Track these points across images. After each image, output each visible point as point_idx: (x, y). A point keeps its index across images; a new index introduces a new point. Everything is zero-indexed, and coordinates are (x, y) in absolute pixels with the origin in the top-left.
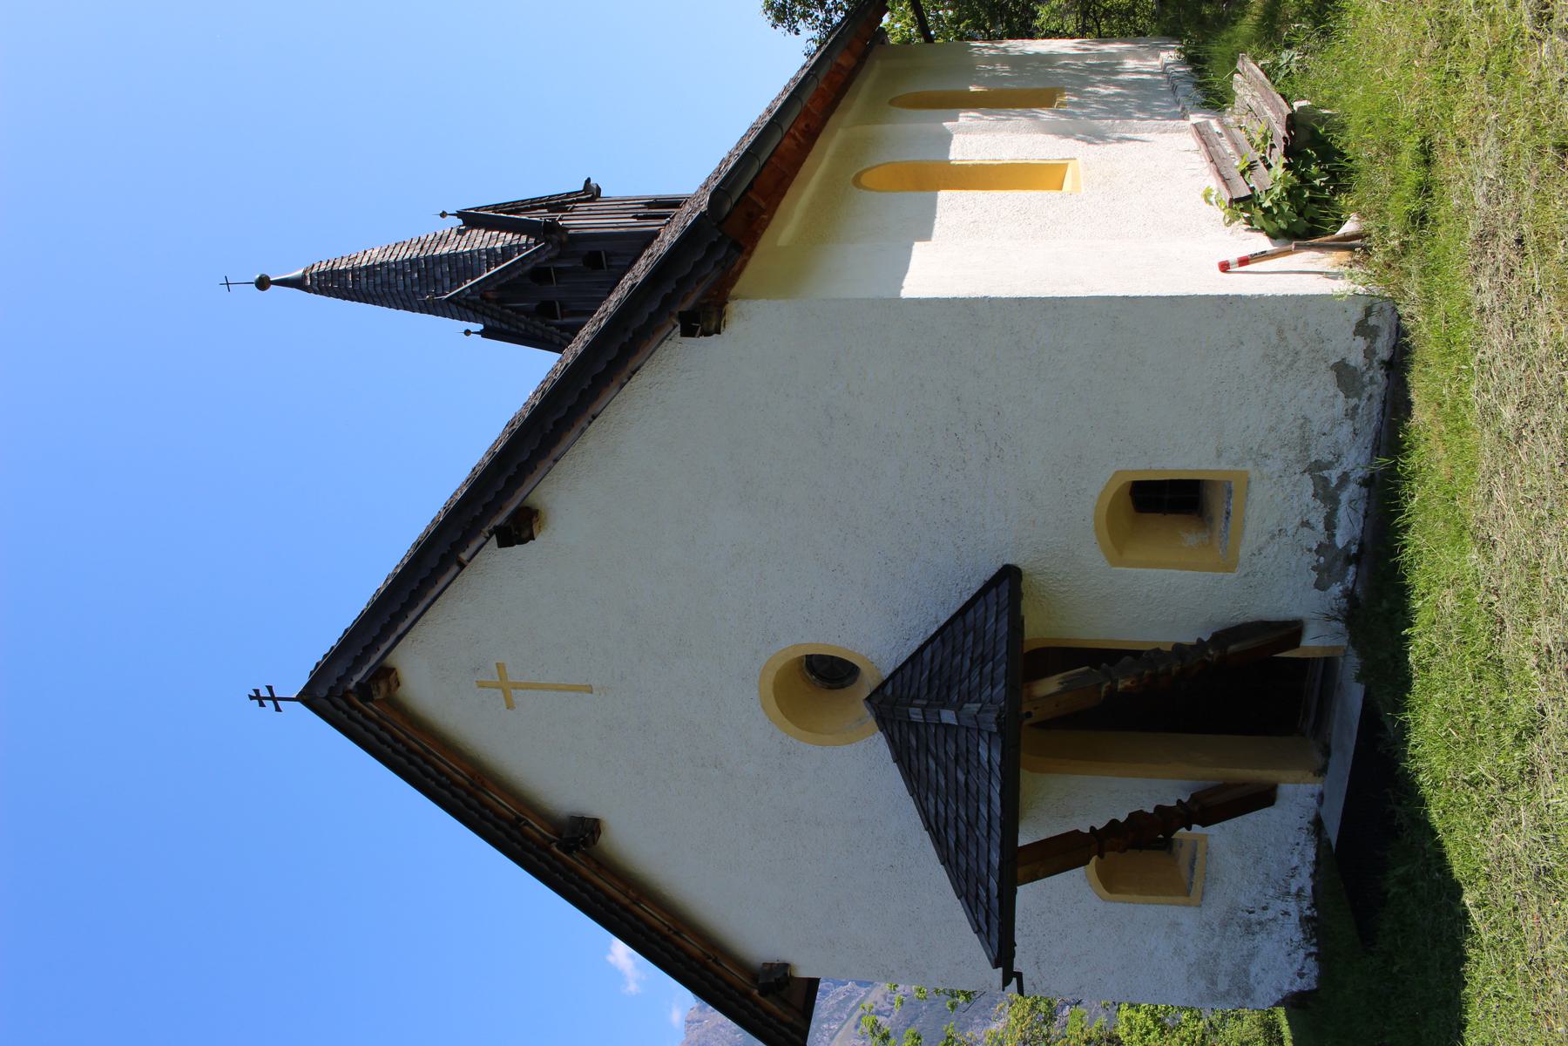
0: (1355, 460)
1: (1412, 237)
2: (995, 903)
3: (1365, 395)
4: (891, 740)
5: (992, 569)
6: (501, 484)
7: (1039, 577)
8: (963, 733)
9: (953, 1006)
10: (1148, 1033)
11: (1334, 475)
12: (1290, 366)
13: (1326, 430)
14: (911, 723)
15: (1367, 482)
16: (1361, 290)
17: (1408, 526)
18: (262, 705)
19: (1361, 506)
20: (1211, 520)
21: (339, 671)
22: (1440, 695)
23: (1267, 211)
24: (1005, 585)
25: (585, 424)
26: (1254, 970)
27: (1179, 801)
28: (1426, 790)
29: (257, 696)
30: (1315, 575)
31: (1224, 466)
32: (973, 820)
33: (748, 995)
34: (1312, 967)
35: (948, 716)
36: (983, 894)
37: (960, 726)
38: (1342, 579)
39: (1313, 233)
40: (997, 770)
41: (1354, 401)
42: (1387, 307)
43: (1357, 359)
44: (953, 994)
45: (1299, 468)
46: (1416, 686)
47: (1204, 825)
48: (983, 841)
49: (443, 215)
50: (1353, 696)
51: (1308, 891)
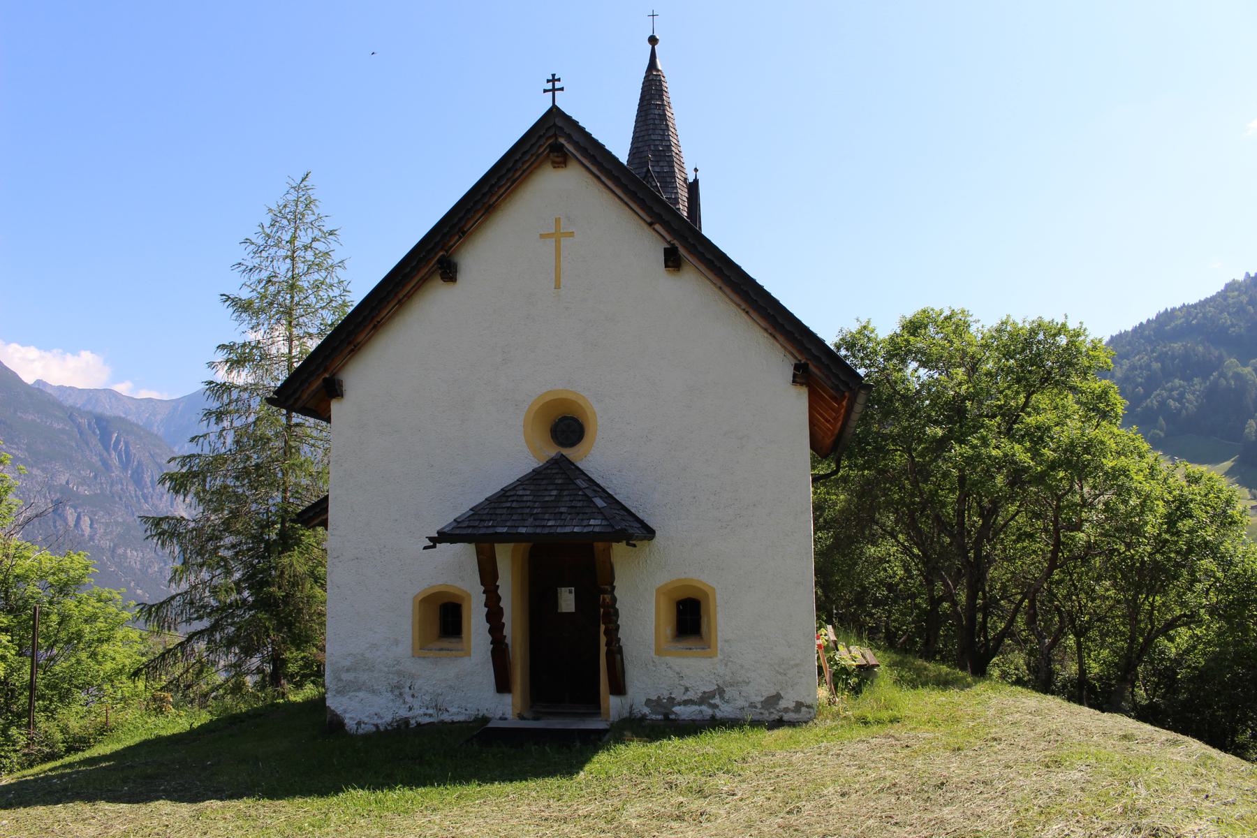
0: (725, 711)
6: (709, 257)
11: (717, 701)
18: (548, 81)
19: (699, 717)
21: (576, 137)
25: (744, 306)
26: (361, 694)
29: (554, 80)
30: (655, 698)
33: (325, 371)
38: (653, 712)
41: (759, 706)
43: (783, 704)
45: (720, 682)
49: (696, 170)
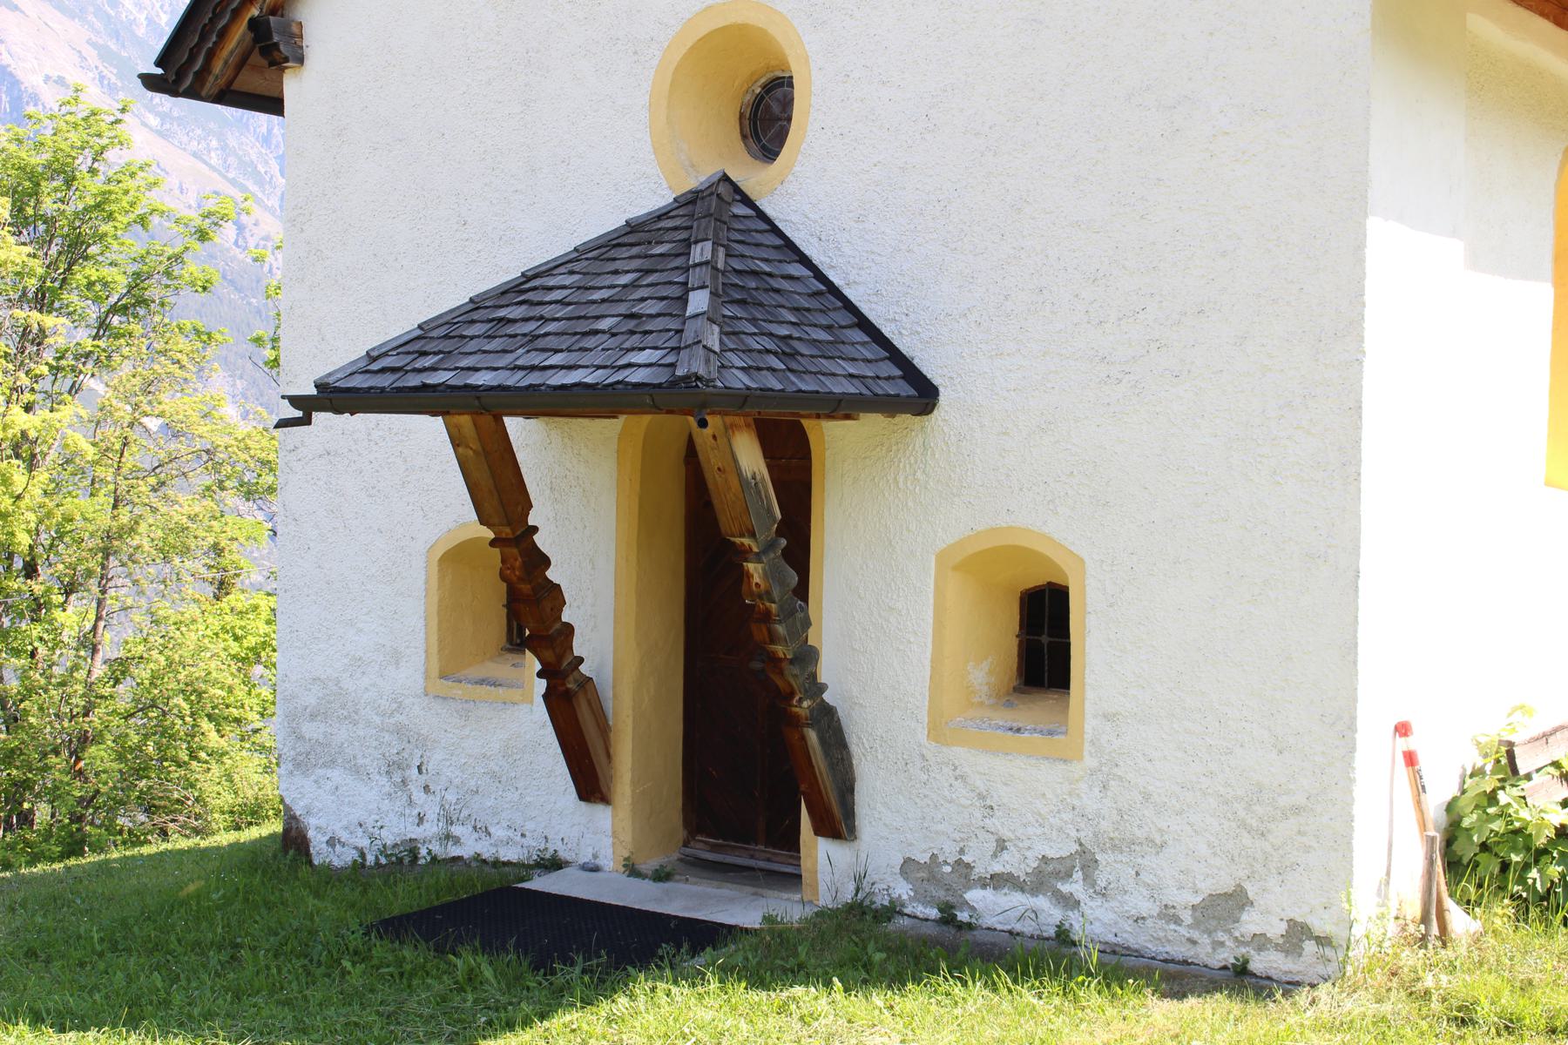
0: (1097, 921)
1: (1436, 1006)
2: (414, 381)
3: (1195, 935)
4: (662, 215)
5: (930, 369)
7: (919, 441)
8: (674, 324)
9: (258, 341)
10: (236, 638)
11: (1074, 887)
12: (1243, 825)
13: (1144, 876)
14: (688, 243)
15: (1063, 937)
16: (1358, 931)
17: (995, 990)
19: (1027, 927)
20: (1009, 705)
22: (743, 1026)
23: (1492, 798)
24: (906, 390)
26: (336, 775)
27: (581, 660)
28: (605, 1007)
30: (923, 858)
31: (1090, 724)
32: (541, 343)
34: (342, 858)
35: (699, 301)
36: (428, 361)
37: (681, 317)
39: (1454, 866)
40: (619, 376)
41: (1187, 917)
42: (1331, 969)
43: (1251, 922)
44: (275, 340)
45: (1086, 835)
46: (758, 996)
47: (545, 697)
48: (507, 360)
50: (743, 910)
51: (455, 851)
